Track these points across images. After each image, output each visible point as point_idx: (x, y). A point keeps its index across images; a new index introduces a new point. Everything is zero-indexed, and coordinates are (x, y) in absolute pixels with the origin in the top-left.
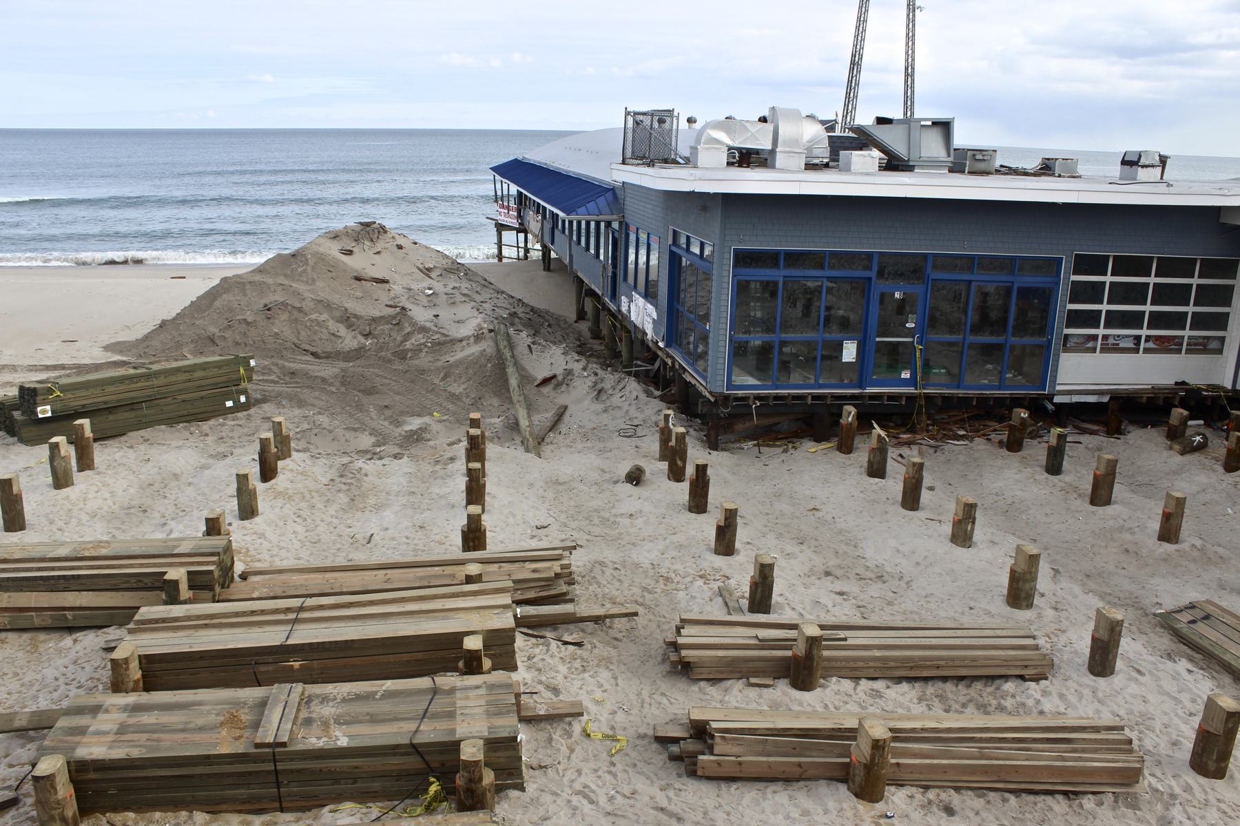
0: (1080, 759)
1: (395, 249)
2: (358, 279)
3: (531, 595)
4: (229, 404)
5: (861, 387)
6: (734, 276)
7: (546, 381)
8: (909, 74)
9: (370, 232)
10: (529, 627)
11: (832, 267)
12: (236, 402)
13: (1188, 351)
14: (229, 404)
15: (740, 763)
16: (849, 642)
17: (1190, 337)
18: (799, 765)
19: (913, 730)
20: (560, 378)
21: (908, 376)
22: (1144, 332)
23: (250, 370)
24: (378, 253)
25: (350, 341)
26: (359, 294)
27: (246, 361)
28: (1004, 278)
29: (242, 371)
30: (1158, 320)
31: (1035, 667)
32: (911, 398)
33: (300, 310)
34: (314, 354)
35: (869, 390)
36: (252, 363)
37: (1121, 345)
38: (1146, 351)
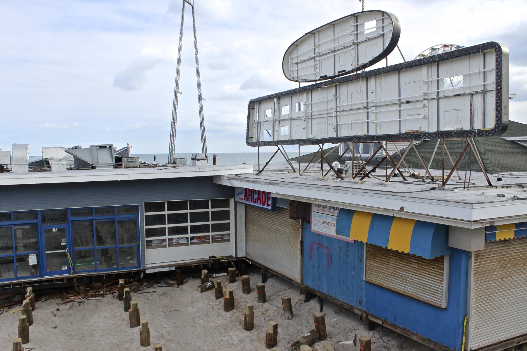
5: (40, 276)
8: (174, 122)
11: (16, 219)
13: (213, 242)
17: (212, 236)
21: (66, 268)
22: (189, 235)
28: (111, 217)
30: (194, 229)
32: (70, 279)
37: (180, 242)
38: (192, 244)
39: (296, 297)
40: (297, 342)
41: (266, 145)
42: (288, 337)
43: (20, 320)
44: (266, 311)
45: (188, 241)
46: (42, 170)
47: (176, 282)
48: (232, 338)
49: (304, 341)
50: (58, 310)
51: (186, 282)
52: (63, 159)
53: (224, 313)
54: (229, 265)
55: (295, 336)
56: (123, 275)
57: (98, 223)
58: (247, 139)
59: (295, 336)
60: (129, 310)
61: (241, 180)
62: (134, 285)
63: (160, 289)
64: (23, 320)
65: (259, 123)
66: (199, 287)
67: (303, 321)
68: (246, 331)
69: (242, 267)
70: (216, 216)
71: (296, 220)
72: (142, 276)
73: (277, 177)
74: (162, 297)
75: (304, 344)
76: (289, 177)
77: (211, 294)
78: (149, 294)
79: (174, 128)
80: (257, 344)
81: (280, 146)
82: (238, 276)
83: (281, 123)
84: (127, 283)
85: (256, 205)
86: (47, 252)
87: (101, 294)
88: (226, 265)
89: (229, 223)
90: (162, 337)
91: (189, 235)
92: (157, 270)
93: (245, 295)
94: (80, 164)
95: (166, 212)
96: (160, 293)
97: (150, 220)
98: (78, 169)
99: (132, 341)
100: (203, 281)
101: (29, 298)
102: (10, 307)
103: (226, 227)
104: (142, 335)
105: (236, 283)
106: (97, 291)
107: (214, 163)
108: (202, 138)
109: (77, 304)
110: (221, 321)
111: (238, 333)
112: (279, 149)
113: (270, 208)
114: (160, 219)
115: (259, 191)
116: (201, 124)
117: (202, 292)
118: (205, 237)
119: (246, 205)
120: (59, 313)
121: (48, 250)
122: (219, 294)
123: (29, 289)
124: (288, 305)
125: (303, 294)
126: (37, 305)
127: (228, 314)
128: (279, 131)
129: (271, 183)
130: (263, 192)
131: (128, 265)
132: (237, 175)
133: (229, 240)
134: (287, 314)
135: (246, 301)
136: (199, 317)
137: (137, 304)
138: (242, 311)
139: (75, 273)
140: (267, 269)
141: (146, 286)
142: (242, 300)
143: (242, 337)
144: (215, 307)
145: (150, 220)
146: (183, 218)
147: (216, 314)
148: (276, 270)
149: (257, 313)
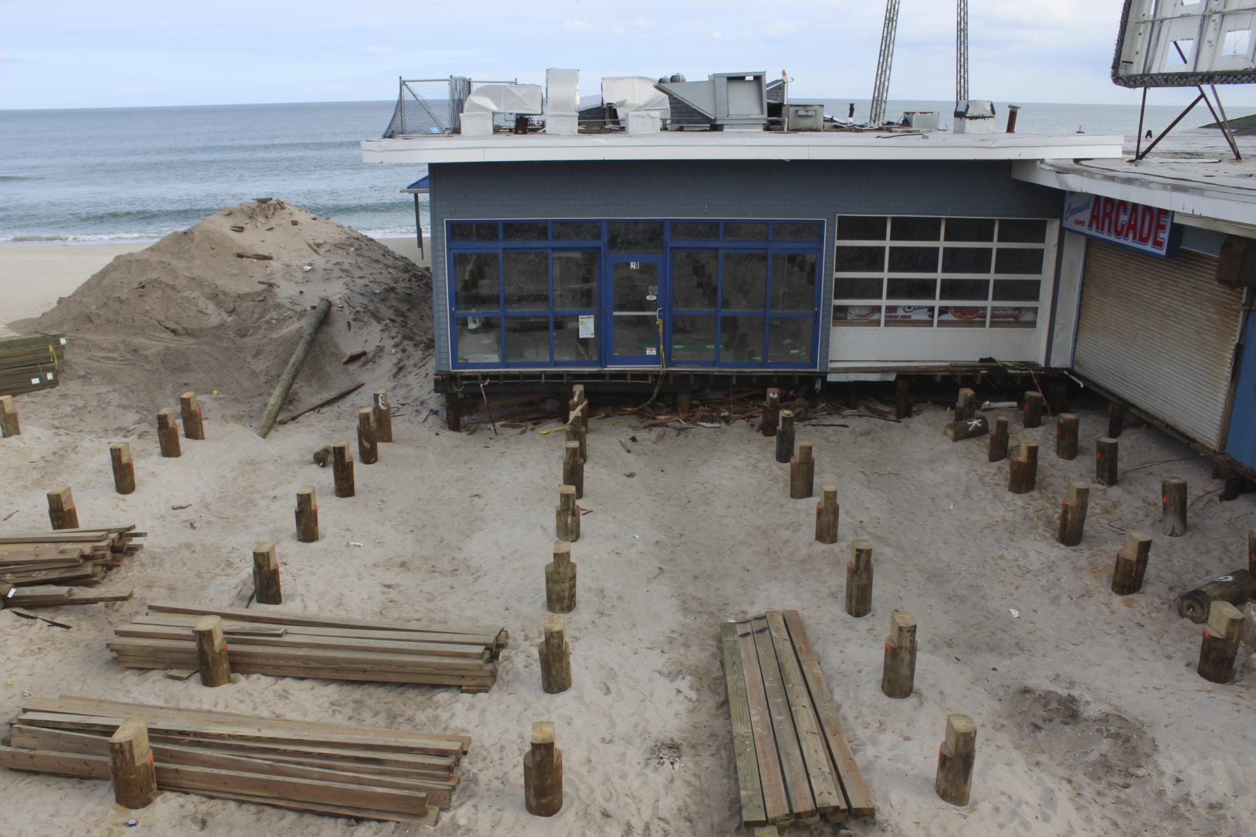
0: (360, 782)
1: (290, 225)
2: (240, 256)
3: (55, 575)
4: (35, 381)
6: (449, 249)
7: (353, 359)
9: (266, 207)
10: (26, 608)
11: (557, 237)
12: (44, 379)
13: (993, 324)
14: (35, 381)
15: (32, 757)
16: (286, 639)
17: (994, 309)
18: (86, 763)
19: (220, 736)
20: (370, 355)
21: (654, 352)
22: (937, 303)
23: (59, 348)
24: (271, 229)
25: (215, 316)
26: (234, 271)
27: (56, 339)
29: (51, 349)
30: (951, 289)
31: (474, 678)
33: (172, 287)
34: (174, 332)
35: (611, 368)
36: (63, 341)
37: (913, 318)
38: (941, 324)
39: (1200, 485)
40: (1197, 592)
41: (1173, 85)
42: (1169, 576)
43: (567, 449)
44: (1115, 505)
45: (932, 316)
46: (602, 130)
47: (894, 410)
48: (1026, 556)
49: (1216, 593)
50: (634, 439)
51: (919, 412)
52: (646, 105)
53: (1009, 496)
54: (1027, 383)
55: (1190, 576)
56: (775, 381)
57: (728, 257)
58: (1116, 67)
59: (1190, 576)
60: (792, 460)
61: (1091, 175)
62: (799, 406)
63: (856, 422)
64: (574, 450)
65: (1156, 23)
66: (950, 426)
67: (1212, 546)
68: (1062, 546)
69: (1059, 393)
70: (1008, 261)
71: (1233, 288)
72: (818, 386)
73: (1194, 171)
74: (861, 439)
75: (1215, 599)
76: (1227, 173)
77: (979, 448)
78: (830, 430)
79: (889, 33)
80: (1088, 579)
81: (1206, 88)
82: (1045, 412)
83: (1229, 21)
84: (784, 400)
85: (1122, 241)
86: (616, 313)
87: (724, 418)
88: (1019, 382)
89: (1038, 283)
90: (863, 528)
91: (937, 303)
92: (852, 377)
93: (1062, 462)
94: (684, 116)
95: (888, 243)
96: (858, 430)
97: (848, 259)
98: (681, 129)
99: (796, 527)
100: (961, 416)
101: (580, 407)
102: (537, 422)
103: (1032, 291)
104: (823, 518)
105: (1041, 429)
106: (714, 410)
107: (1010, 128)
108: (959, 61)
109: (674, 433)
110: (1001, 512)
111: (1043, 546)
112: (1203, 95)
113: (1163, 252)
114: (872, 259)
115: (1135, 206)
116: (959, 23)
117: (955, 440)
118: (974, 310)
119: (1090, 240)
120: (635, 447)
121: (622, 308)
122: (999, 450)
123: (578, 389)
124: (1177, 503)
125: (1221, 478)
126: (592, 423)
127: (1019, 500)
128: (1216, 45)
129: (1179, 187)
130: (1147, 209)
131: (788, 359)
132: (1077, 161)
133: (1033, 324)
134: (1172, 521)
135: (1068, 476)
136: (948, 496)
137: (810, 448)
138: (1054, 497)
139: (668, 366)
140: (1126, 405)
141: (823, 409)
142: (1054, 472)
143: (1053, 556)
144: (986, 479)
145: (848, 259)
146: (926, 260)
147: (990, 496)
148: (1152, 411)
149: (1095, 506)
